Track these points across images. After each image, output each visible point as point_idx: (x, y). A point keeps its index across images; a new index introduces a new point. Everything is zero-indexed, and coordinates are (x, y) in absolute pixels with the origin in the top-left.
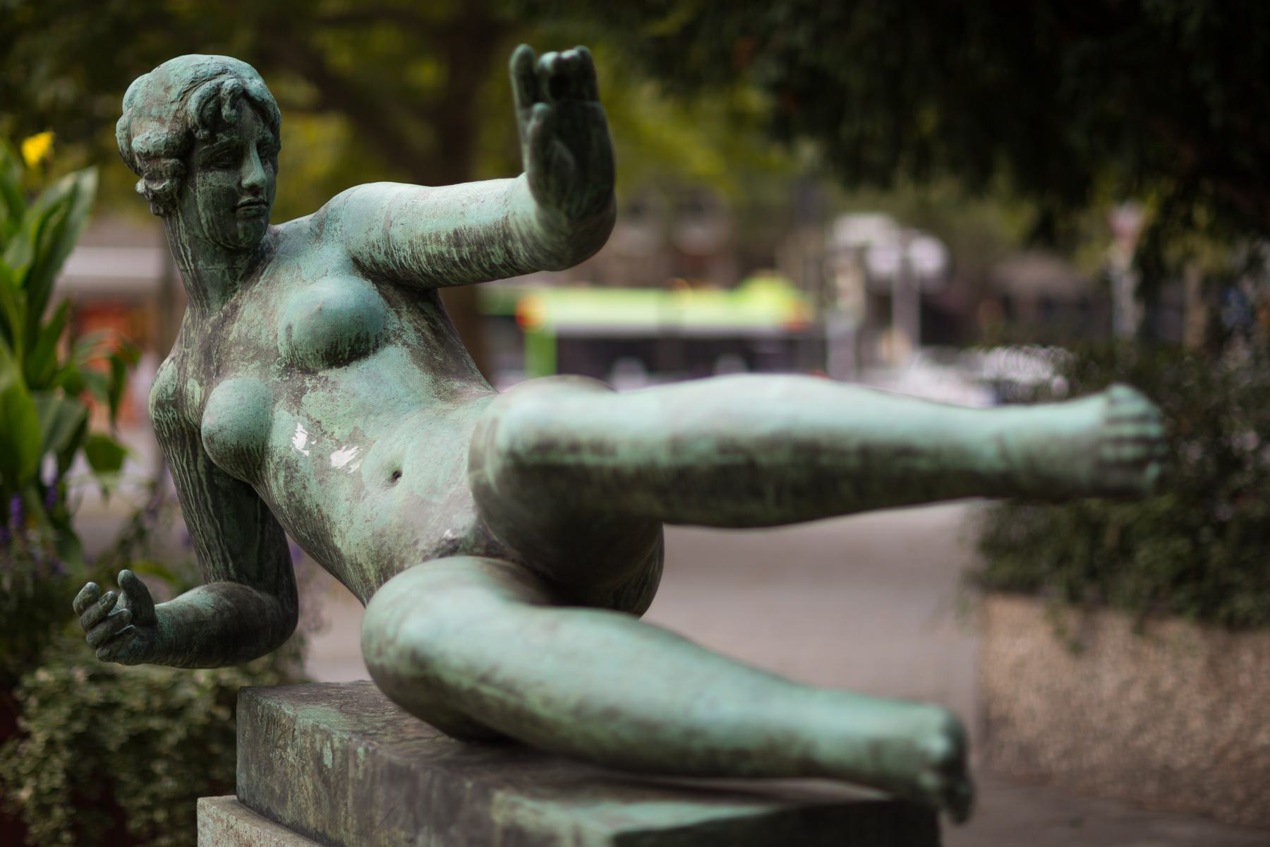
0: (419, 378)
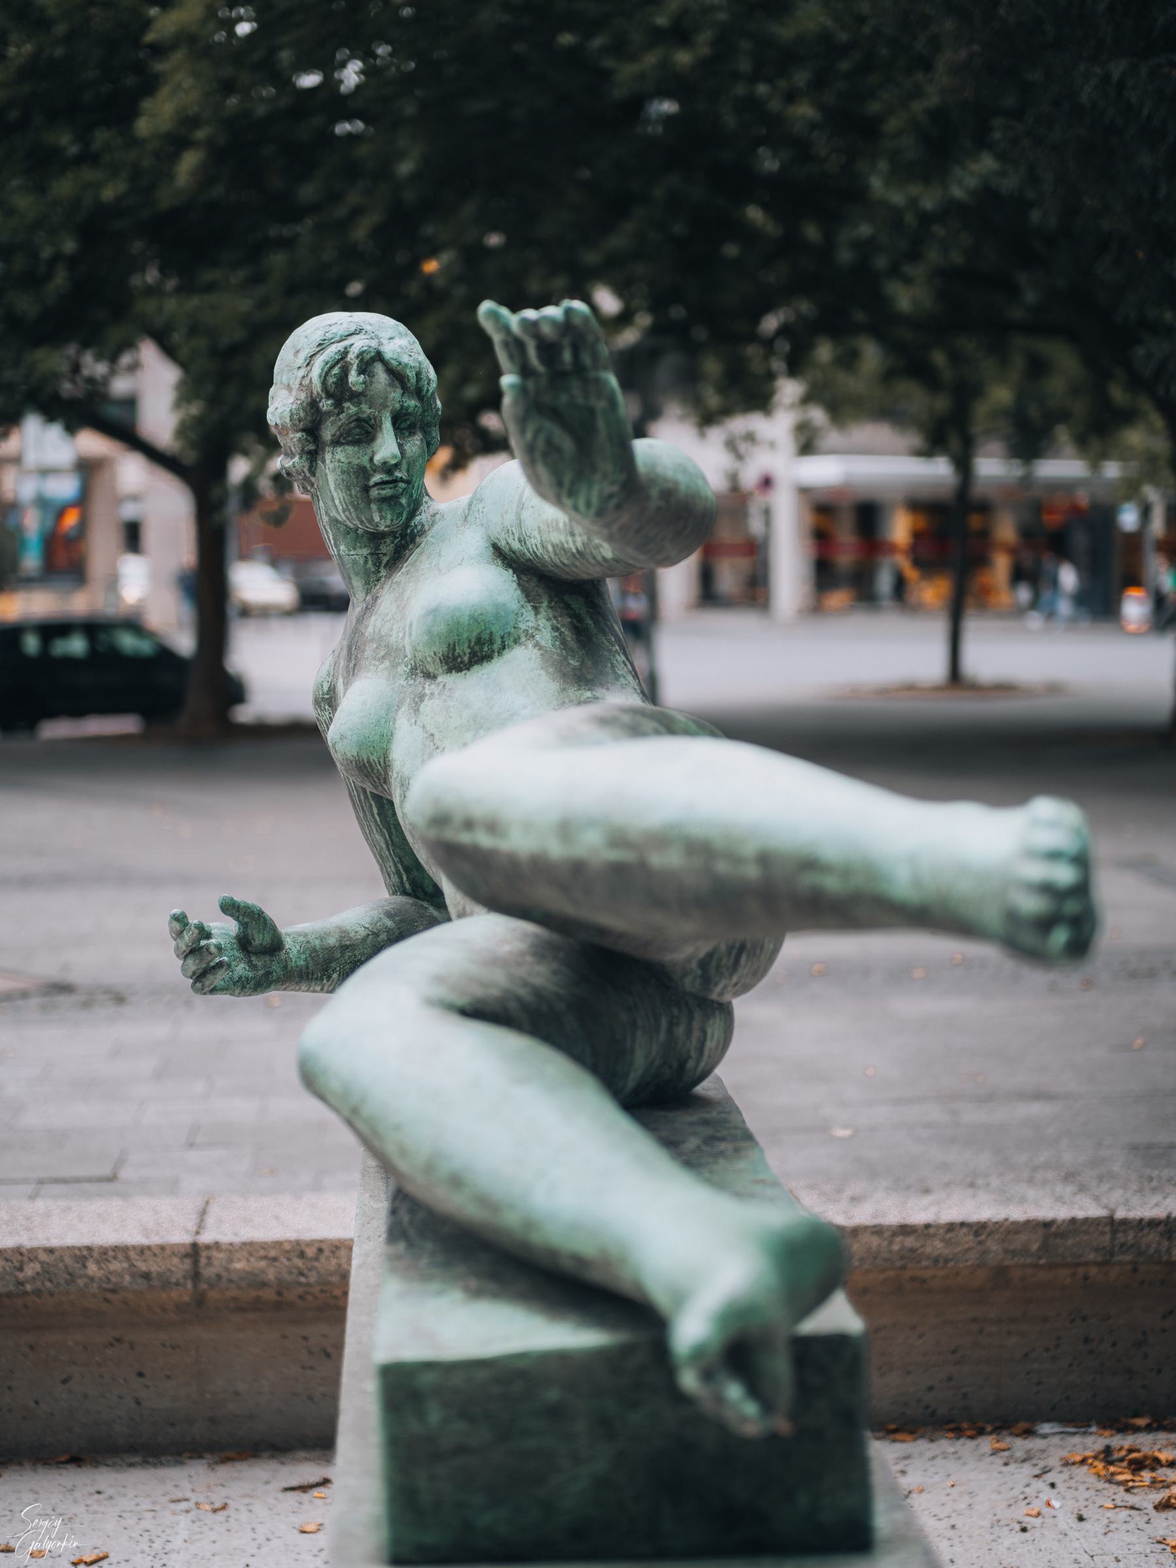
0: (548, 684)
